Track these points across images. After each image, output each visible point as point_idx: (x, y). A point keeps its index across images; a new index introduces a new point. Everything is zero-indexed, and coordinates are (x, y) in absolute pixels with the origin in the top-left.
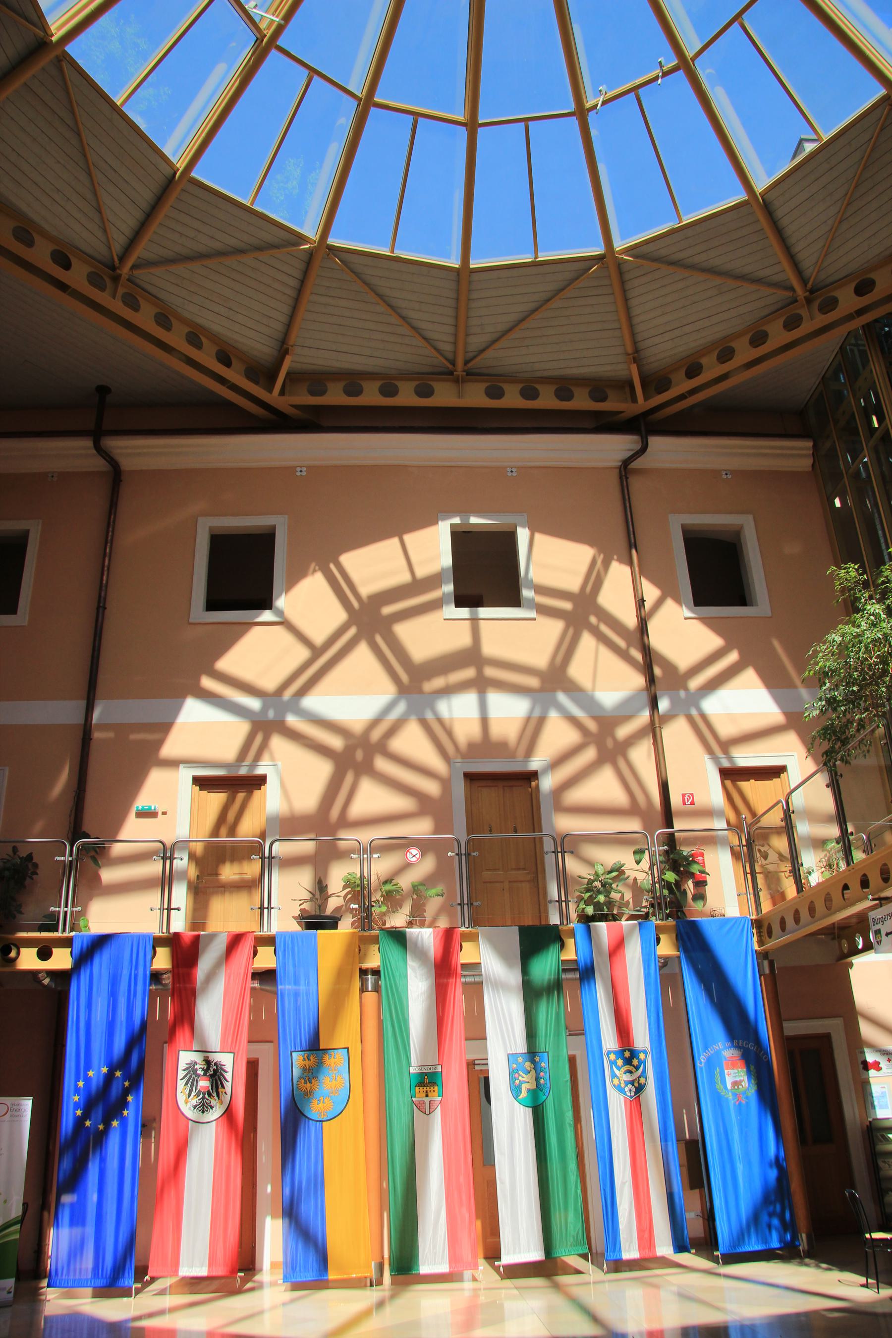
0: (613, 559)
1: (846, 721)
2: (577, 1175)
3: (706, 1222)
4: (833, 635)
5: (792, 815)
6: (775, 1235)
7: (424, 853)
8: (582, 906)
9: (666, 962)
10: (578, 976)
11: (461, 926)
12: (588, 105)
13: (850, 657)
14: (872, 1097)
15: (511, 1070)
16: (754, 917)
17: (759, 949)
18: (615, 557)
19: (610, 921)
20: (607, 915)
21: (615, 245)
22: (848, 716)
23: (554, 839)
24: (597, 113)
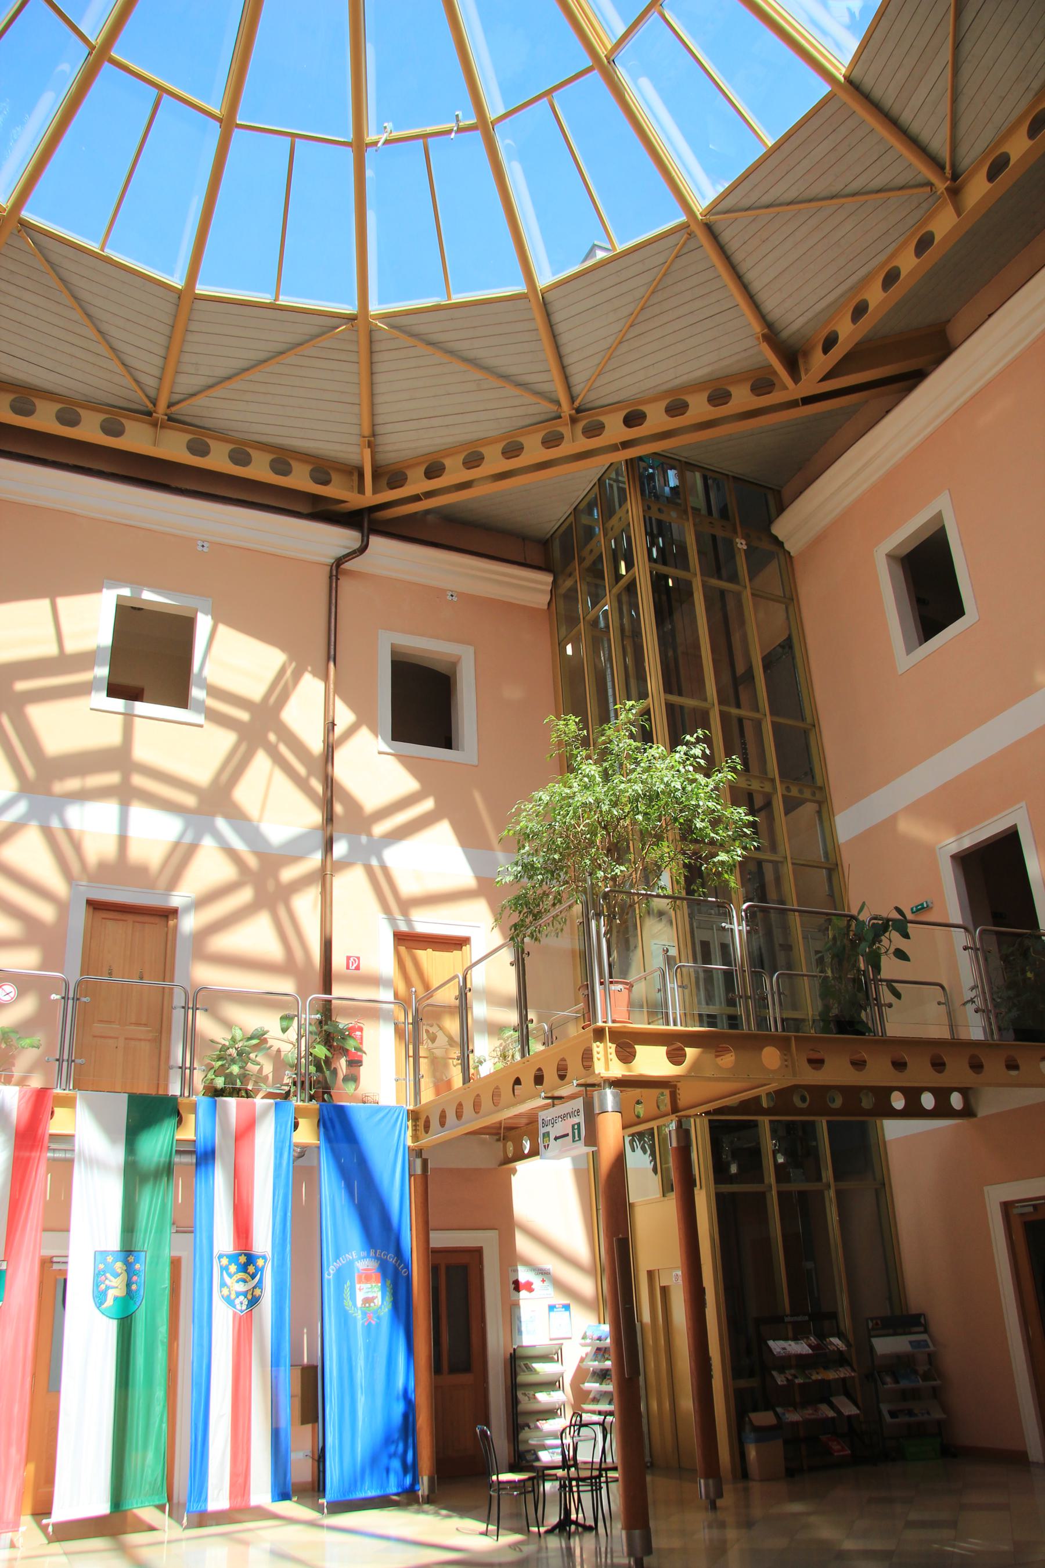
0: (306, 670)
1: (541, 892)
2: (164, 1406)
3: (316, 1463)
4: (541, 793)
5: (469, 994)
6: (393, 1479)
7: (21, 993)
8: (211, 1075)
9: (303, 1152)
10: (194, 1161)
11: (55, 1087)
12: (370, 138)
13: (556, 821)
14: (520, 1322)
15: (97, 1271)
16: (411, 1107)
17: (412, 1145)
18: (309, 668)
19: (242, 1097)
20: (240, 1089)
21: (370, 308)
22: (545, 887)
23: (186, 993)
24: (376, 151)
